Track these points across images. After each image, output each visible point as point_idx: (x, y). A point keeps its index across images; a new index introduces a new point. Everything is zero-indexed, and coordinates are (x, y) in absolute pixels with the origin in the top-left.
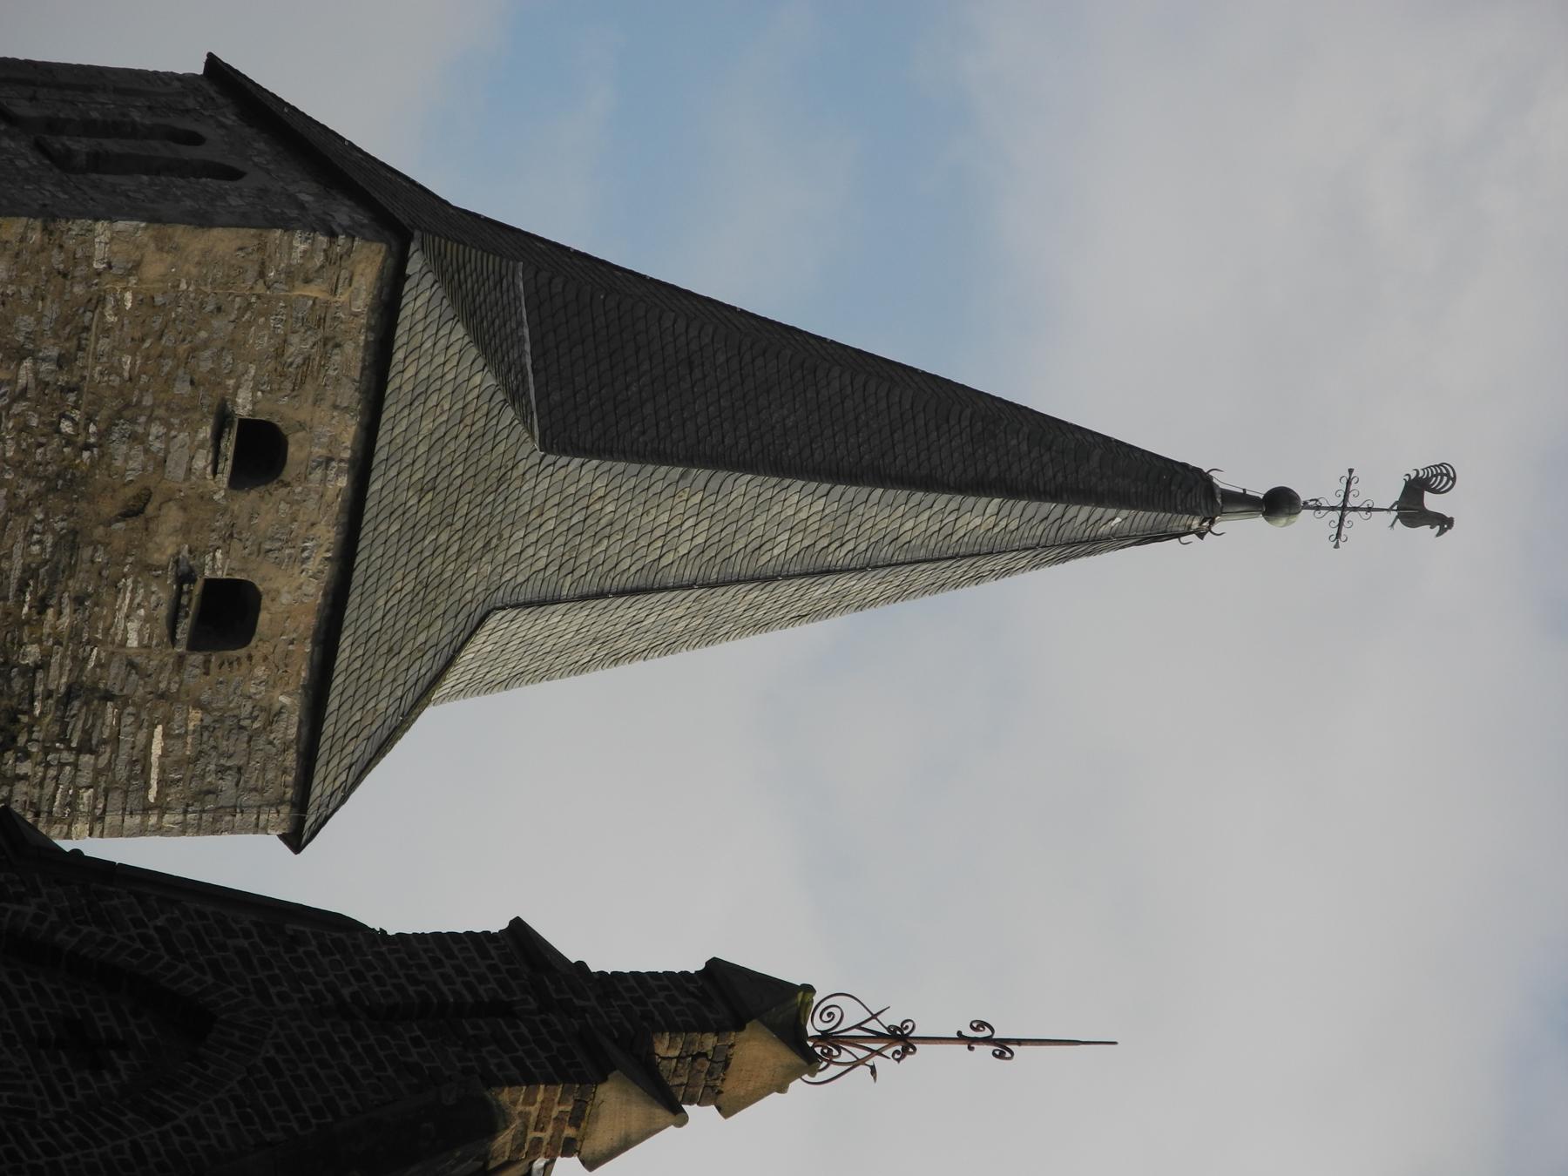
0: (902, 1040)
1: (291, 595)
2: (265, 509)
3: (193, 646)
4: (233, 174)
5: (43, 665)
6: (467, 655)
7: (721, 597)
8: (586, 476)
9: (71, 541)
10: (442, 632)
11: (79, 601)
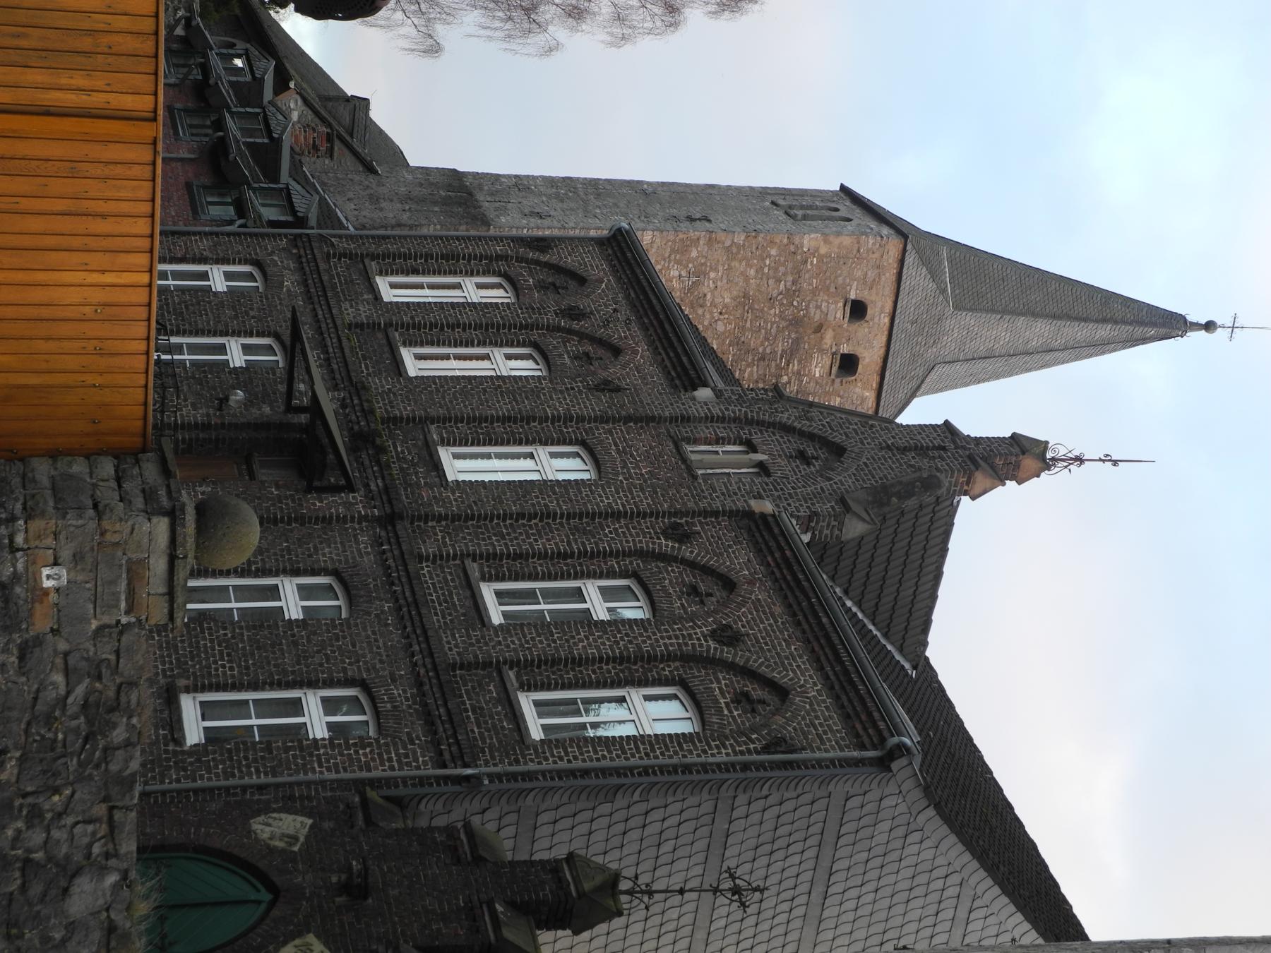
0: (1080, 460)
1: (870, 357)
2: (861, 329)
3: (837, 376)
4: (849, 220)
5: (789, 382)
6: (928, 380)
7: (1014, 359)
8: (968, 319)
9: (797, 342)
10: (920, 372)
11: (799, 362)
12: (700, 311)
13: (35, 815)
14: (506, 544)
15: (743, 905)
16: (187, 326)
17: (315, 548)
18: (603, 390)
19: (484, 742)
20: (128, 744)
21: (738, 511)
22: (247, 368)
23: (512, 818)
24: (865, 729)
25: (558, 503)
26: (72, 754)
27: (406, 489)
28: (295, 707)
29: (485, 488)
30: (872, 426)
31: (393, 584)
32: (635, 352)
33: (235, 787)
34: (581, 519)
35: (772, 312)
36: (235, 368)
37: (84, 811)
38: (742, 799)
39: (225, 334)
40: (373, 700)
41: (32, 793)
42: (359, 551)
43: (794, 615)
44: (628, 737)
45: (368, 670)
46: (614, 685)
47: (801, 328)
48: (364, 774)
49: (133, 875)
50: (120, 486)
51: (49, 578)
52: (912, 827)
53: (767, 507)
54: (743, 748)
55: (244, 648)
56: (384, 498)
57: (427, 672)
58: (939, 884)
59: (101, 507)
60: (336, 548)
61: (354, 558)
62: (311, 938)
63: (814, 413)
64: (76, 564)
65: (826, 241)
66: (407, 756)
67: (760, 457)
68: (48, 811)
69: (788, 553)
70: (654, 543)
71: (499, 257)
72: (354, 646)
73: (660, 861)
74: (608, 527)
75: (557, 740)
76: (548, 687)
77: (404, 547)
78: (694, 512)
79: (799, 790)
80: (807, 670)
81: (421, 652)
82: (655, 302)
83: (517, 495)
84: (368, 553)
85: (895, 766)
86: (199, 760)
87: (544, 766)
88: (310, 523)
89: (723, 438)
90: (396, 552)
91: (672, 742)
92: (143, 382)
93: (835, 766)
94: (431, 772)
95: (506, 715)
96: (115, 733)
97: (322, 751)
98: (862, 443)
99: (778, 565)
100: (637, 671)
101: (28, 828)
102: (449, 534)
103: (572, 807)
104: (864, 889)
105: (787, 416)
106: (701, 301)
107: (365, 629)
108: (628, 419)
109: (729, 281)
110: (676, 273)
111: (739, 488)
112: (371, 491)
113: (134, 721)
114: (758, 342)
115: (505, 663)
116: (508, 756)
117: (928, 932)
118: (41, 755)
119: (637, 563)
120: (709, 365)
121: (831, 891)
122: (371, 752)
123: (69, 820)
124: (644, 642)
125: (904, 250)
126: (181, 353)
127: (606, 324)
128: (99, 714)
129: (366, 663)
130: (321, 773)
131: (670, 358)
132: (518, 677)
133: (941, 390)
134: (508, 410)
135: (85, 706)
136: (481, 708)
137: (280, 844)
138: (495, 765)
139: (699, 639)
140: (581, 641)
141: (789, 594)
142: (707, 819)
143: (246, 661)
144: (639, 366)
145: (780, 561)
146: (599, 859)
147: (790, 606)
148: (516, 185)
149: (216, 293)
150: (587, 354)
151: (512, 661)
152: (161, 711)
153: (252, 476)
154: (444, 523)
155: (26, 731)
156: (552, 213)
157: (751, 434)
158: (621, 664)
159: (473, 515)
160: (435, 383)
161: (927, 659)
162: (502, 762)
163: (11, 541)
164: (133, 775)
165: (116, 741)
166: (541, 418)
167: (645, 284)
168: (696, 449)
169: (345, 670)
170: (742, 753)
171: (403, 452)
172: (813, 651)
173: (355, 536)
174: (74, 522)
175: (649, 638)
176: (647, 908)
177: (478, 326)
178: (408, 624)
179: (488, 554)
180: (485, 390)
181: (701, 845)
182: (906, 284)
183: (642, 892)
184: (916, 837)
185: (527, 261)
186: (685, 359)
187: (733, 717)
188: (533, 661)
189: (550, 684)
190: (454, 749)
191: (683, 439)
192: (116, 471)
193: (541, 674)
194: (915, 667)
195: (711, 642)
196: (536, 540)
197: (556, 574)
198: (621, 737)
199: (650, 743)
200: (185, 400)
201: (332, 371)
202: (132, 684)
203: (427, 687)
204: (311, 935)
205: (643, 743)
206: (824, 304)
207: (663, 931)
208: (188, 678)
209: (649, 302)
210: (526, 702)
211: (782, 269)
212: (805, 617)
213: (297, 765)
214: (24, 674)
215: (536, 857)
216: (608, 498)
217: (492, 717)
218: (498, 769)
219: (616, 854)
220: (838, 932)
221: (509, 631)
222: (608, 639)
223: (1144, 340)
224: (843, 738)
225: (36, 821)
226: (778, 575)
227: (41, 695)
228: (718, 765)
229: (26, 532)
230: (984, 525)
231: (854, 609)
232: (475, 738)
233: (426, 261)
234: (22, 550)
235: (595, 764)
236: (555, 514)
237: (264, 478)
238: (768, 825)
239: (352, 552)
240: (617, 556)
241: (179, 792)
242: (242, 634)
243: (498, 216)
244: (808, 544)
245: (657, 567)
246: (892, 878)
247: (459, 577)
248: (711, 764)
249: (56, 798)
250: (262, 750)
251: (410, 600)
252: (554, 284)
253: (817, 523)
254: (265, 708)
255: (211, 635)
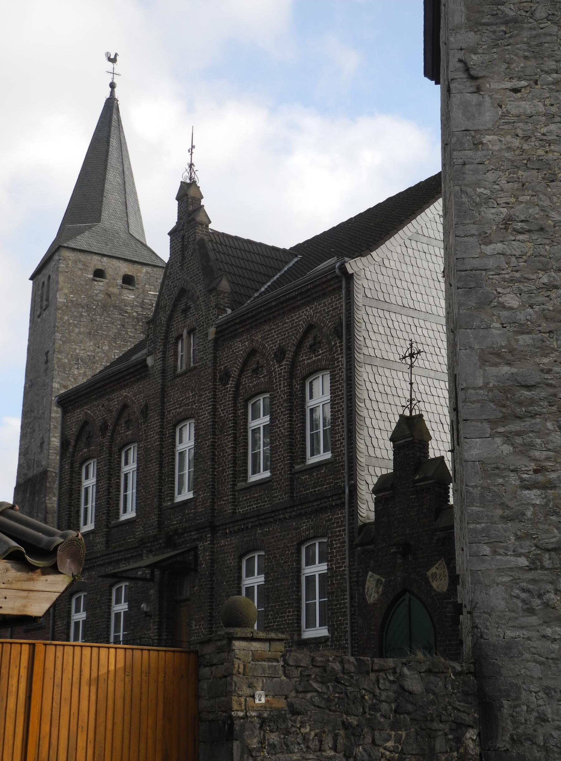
0: (191, 165)
2: (110, 272)
3: (134, 286)
4: (49, 277)
5: (137, 312)
6: (137, 237)
7: (128, 191)
8: (105, 215)
9: (115, 307)
11: (126, 306)
12: (97, 358)
13: (374, 708)
14: (228, 468)
15: (419, 352)
16: (105, 633)
17: (227, 567)
18: (147, 415)
19: (332, 482)
20: (342, 662)
21: (214, 346)
22: (129, 602)
23: (371, 468)
24: (331, 286)
25: (207, 440)
26: (346, 689)
27: (197, 520)
28: (310, 579)
29: (198, 478)
30: (170, 273)
31: (247, 528)
32: (126, 396)
33: (351, 611)
34: (215, 428)
35: (98, 320)
36: (128, 608)
37: (373, 684)
38: (365, 351)
39: (109, 613)
40: (308, 539)
41: (364, 709)
42: (229, 545)
43: (270, 319)
44: (331, 408)
45: (292, 542)
46: (304, 415)
47: (108, 305)
48: (347, 544)
49: (404, 660)
50: (215, 665)
51: (261, 699)
52: (381, 264)
53: (212, 331)
54: (339, 349)
55: (279, 605)
56: (201, 531)
57: (294, 511)
58: (410, 251)
59: (226, 674)
60: (227, 557)
61: (233, 548)
62: (429, 573)
63: (162, 303)
64: (254, 686)
65: (61, 290)
66: (338, 523)
67: (185, 333)
68: (372, 701)
69: (237, 321)
70: (230, 391)
71: (72, 467)
72: (279, 548)
73: (395, 394)
74: (220, 414)
75: (332, 445)
76: (304, 448)
77: (229, 521)
78: (214, 369)
79: (362, 321)
80: (299, 314)
81: (284, 514)
82: (99, 385)
83: (202, 461)
84: (231, 540)
85: (350, 271)
86: (336, 629)
87: (345, 452)
88: (213, 570)
89: (174, 352)
90: (231, 525)
91: (335, 386)
92: (163, 653)
93: (350, 302)
94: (346, 510)
95: (318, 471)
96: (337, 669)
97: (334, 566)
98: (179, 279)
99: (243, 326)
100: (297, 402)
101: (380, 711)
102: (222, 497)
103: (366, 438)
104: (412, 289)
105: (164, 319)
106: (92, 358)
107: (270, 543)
108: (163, 402)
109: (81, 342)
110: (76, 370)
111: (202, 345)
112: (198, 538)
113: (331, 659)
114: (114, 327)
115: (291, 470)
116: (340, 470)
117: (434, 257)
118: (346, 704)
119: (240, 400)
120: (134, 358)
121: (412, 307)
122: (335, 540)
123: (377, 691)
124: (282, 398)
125: (67, 248)
126: (119, 636)
127: (111, 411)
128: (327, 676)
129: (289, 543)
130: (345, 567)
131: (130, 378)
132: (298, 464)
133: (143, 231)
134: (156, 465)
135: (323, 683)
136: (314, 483)
137: (381, 589)
138: (344, 477)
139: (281, 369)
140: (280, 431)
141: (259, 321)
142: (375, 369)
143: (286, 604)
144: (133, 395)
145: (241, 325)
146: (394, 425)
147: (265, 321)
148: (24, 455)
149: (87, 617)
150: (126, 422)
151: (290, 467)
152: (310, 648)
153: (188, 600)
154: (216, 500)
155: (334, 711)
156: (41, 436)
157: (173, 337)
158: (293, 410)
159: (212, 485)
160: (140, 503)
161: (291, 249)
162: (342, 474)
163: (242, 718)
164: (357, 660)
165: (340, 668)
166: (161, 448)
167: (89, 390)
168: (179, 366)
169: (292, 554)
170: (341, 350)
171: (177, 521)
172: (289, 310)
173: (221, 546)
174: (233, 687)
175: (280, 395)
176: (419, 402)
177: (109, 479)
178: (269, 520)
179: (233, 477)
180: (145, 477)
181: (387, 372)
182: (85, 247)
183: (411, 404)
184: (386, 262)
185: (74, 452)
186: (131, 370)
187: (323, 353)
188: (290, 456)
189: (303, 448)
190: (335, 498)
191: (174, 373)
192: (207, 667)
193: (297, 452)
194: (296, 256)
195: (283, 363)
196: (226, 452)
197: (244, 442)
198: (331, 412)
199: (335, 397)
200: (145, 634)
201: (132, 557)
202: (313, 659)
203: (303, 511)
204: (427, 573)
205: (335, 400)
206: (95, 292)
207: (430, 393)
208: (294, 634)
209: (99, 388)
210: (312, 460)
211: (75, 314)
212: (271, 313)
213: (340, 579)
214: (306, 712)
215: (392, 457)
216: (205, 414)
217: (319, 478)
218: (346, 476)
219: (391, 416)
220: (432, 303)
221: (274, 468)
222: (280, 416)
223: (119, 121)
224: (335, 298)
225: (377, 707)
226: (248, 327)
227: (317, 704)
228: (347, 362)
229: (238, 711)
230: (224, 218)
231: (266, 286)
232: (330, 487)
233: (72, 506)
234: (246, 712)
235: (345, 426)
236: (213, 442)
237: (188, 594)
238: (378, 337)
239: (230, 548)
240: (236, 410)
241: (352, 639)
242: (272, 606)
243: (42, 466)
244: (232, 310)
245: (242, 389)
246: (407, 275)
247: (245, 493)
248: (347, 366)
249: (366, 697)
250: (332, 597)
251: (256, 519)
252: (87, 438)
253: (221, 305)
254: (310, 595)
255: (271, 623)
